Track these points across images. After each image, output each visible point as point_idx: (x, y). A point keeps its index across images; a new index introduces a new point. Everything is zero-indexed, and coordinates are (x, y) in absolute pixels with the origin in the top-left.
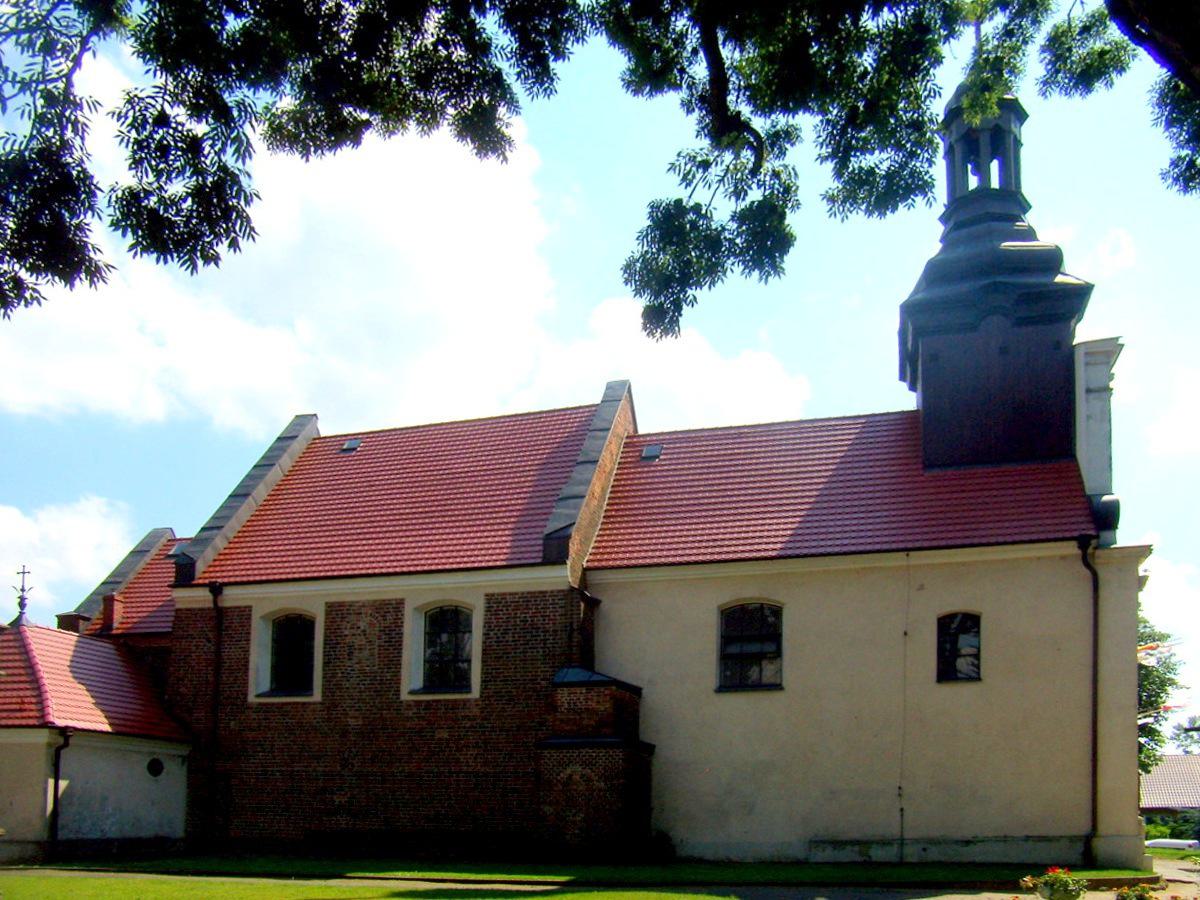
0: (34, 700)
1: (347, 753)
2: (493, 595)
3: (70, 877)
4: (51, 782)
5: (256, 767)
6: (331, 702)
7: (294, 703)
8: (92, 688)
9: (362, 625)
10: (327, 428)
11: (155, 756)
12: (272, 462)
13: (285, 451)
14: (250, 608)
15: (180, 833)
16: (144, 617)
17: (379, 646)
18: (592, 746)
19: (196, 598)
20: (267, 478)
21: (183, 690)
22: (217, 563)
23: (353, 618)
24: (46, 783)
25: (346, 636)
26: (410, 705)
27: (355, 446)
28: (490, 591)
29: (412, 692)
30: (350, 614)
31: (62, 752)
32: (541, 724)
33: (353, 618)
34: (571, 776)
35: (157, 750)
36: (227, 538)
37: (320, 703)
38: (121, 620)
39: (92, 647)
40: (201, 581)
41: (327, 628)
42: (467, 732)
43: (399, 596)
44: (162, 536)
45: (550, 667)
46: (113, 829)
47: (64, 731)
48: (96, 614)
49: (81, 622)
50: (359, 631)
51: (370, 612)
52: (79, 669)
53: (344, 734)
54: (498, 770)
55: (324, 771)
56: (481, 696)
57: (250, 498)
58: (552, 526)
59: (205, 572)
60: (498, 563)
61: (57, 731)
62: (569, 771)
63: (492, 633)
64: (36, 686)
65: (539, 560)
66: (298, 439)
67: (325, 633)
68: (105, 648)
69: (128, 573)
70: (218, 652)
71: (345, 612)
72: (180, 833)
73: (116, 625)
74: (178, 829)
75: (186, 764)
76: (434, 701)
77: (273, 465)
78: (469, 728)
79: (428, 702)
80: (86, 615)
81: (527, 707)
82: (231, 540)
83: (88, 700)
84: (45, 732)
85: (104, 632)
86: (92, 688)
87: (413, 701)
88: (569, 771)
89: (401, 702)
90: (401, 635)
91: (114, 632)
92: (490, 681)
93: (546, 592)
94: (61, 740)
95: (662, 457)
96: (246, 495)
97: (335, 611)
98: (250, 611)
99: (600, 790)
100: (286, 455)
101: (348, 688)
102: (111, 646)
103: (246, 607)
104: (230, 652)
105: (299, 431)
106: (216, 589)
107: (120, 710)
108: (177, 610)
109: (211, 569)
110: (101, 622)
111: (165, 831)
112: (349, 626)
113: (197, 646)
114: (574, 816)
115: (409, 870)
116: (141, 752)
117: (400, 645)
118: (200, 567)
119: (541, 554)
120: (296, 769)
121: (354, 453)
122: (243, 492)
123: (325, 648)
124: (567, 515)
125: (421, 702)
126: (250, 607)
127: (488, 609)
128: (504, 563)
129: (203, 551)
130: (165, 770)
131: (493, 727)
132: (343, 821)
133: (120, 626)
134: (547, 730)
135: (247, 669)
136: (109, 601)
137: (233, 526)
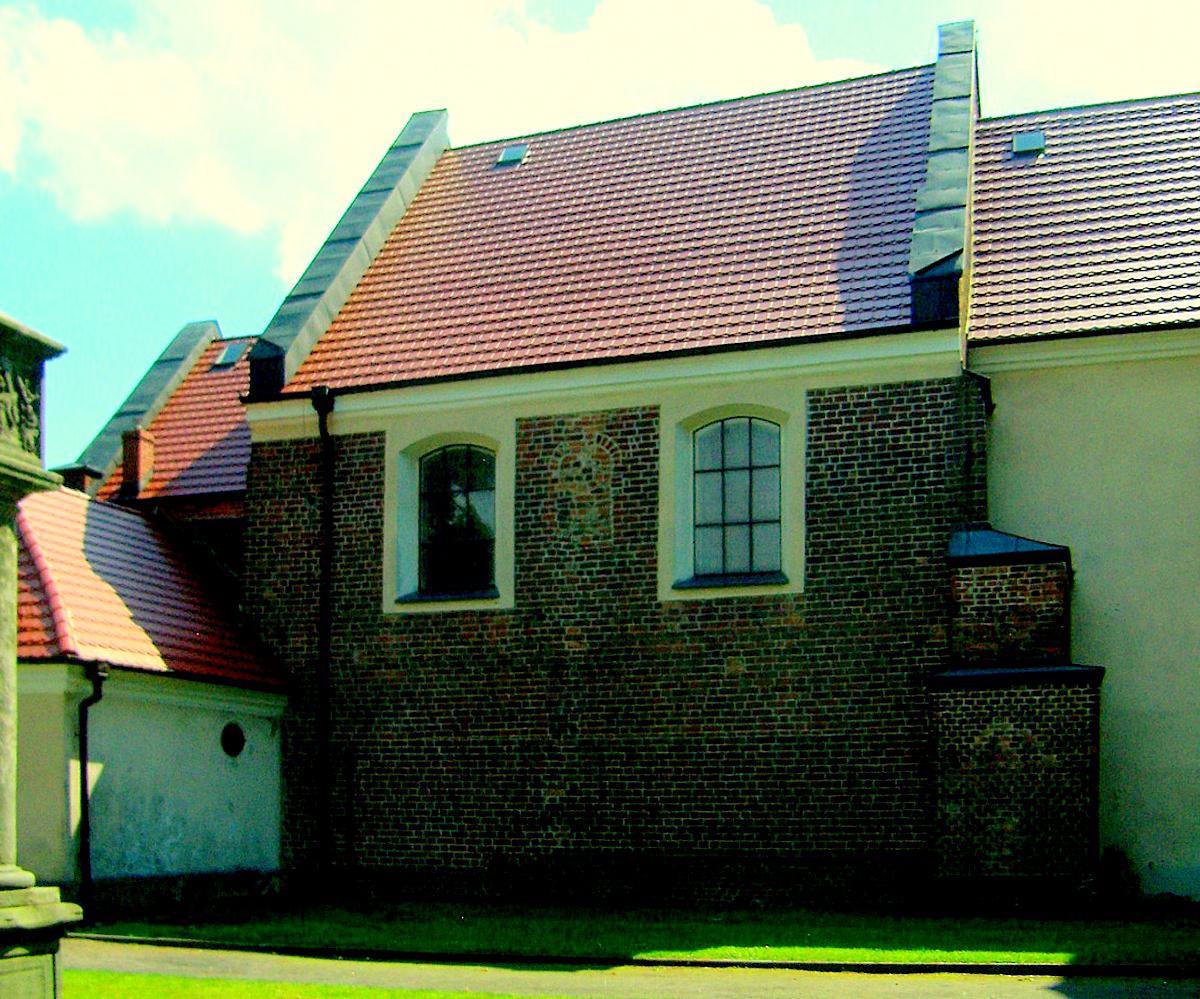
0: (36, 610)
1: (562, 706)
2: (821, 392)
3: (170, 961)
4: (75, 765)
5: (401, 736)
6: (531, 610)
7: (465, 613)
8: (127, 591)
9: (583, 458)
10: (462, 132)
11: (232, 719)
12: (388, 186)
13: (405, 166)
14: (379, 436)
15: (273, 862)
16: (174, 479)
17: (617, 498)
18: (1033, 681)
19: (289, 420)
20: (383, 209)
21: (268, 593)
22: (317, 357)
23: (565, 445)
24: (67, 769)
25: (555, 481)
26: (675, 612)
27: (234, 360)
28: (815, 385)
29: (679, 586)
30: (561, 439)
31: (92, 710)
32: (920, 641)
33: (565, 445)
34: (994, 740)
35: (235, 708)
36: (330, 315)
37: (510, 612)
38: (151, 475)
39: (111, 519)
40: (295, 389)
41: (521, 468)
42: (782, 660)
43: (648, 402)
44: (202, 334)
45: (934, 530)
46: (174, 856)
47: (92, 670)
48: (111, 467)
49: (88, 479)
50: (579, 471)
51: (597, 433)
52: (97, 554)
53: (558, 667)
54: (842, 732)
55: (522, 742)
56: (807, 591)
57: (361, 243)
58: (921, 258)
59: (298, 374)
60: (830, 330)
61: (78, 669)
62: (990, 733)
63: (822, 466)
64: (36, 584)
65: (908, 321)
66: (423, 147)
67: (518, 477)
68: (125, 521)
69: (153, 397)
70: (328, 518)
71: (552, 435)
72: (273, 862)
73: (143, 483)
74: (267, 853)
75: (278, 734)
76: (719, 601)
77: (390, 189)
78: (785, 652)
79: (709, 602)
80: (96, 469)
81: (893, 608)
82: (337, 317)
83: (120, 611)
84: (62, 669)
85: (125, 496)
86: (127, 591)
87: (685, 603)
88: (990, 733)
89: (659, 605)
90: (654, 474)
91: (142, 496)
92: (821, 560)
93: (919, 384)
94: (89, 689)
95: (1048, 151)
96: (354, 239)
97: (536, 435)
98: (382, 441)
99: (1050, 770)
100: (407, 173)
101: (561, 582)
102: (138, 519)
103: (375, 434)
104: (349, 520)
105: (424, 136)
106: (323, 400)
107: (174, 631)
108: (255, 446)
109: (310, 367)
110: (121, 479)
111: (250, 860)
112: (560, 460)
113: (291, 511)
114: (1002, 821)
115: (779, 942)
116: (212, 706)
117: (654, 495)
118: (292, 364)
119: (908, 312)
120: (471, 739)
121: (518, 167)
122: (347, 234)
123: (517, 505)
124: (942, 238)
125: (697, 603)
126: (383, 433)
127: (814, 421)
128: (841, 329)
129: (294, 335)
130: (246, 745)
131: (829, 650)
132: (558, 837)
133: (149, 486)
134: (930, 653)
135: (380, 551)
136: (131, 440)
137: (337, 293)
